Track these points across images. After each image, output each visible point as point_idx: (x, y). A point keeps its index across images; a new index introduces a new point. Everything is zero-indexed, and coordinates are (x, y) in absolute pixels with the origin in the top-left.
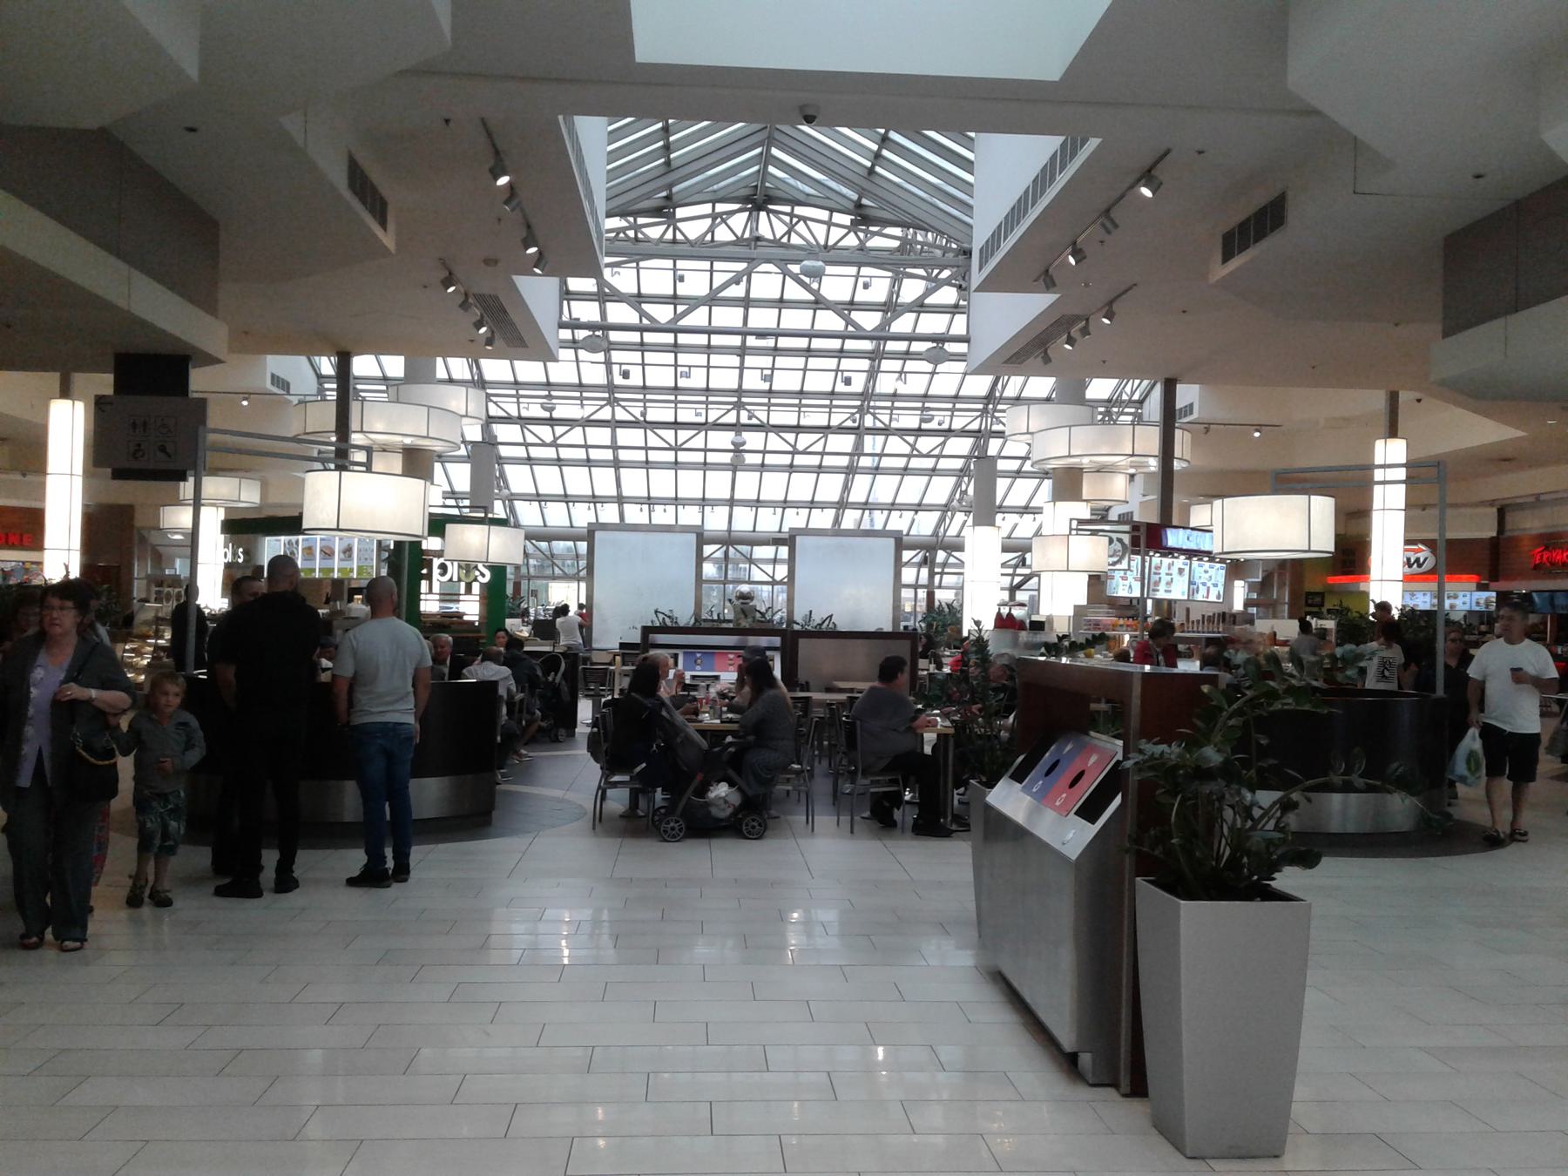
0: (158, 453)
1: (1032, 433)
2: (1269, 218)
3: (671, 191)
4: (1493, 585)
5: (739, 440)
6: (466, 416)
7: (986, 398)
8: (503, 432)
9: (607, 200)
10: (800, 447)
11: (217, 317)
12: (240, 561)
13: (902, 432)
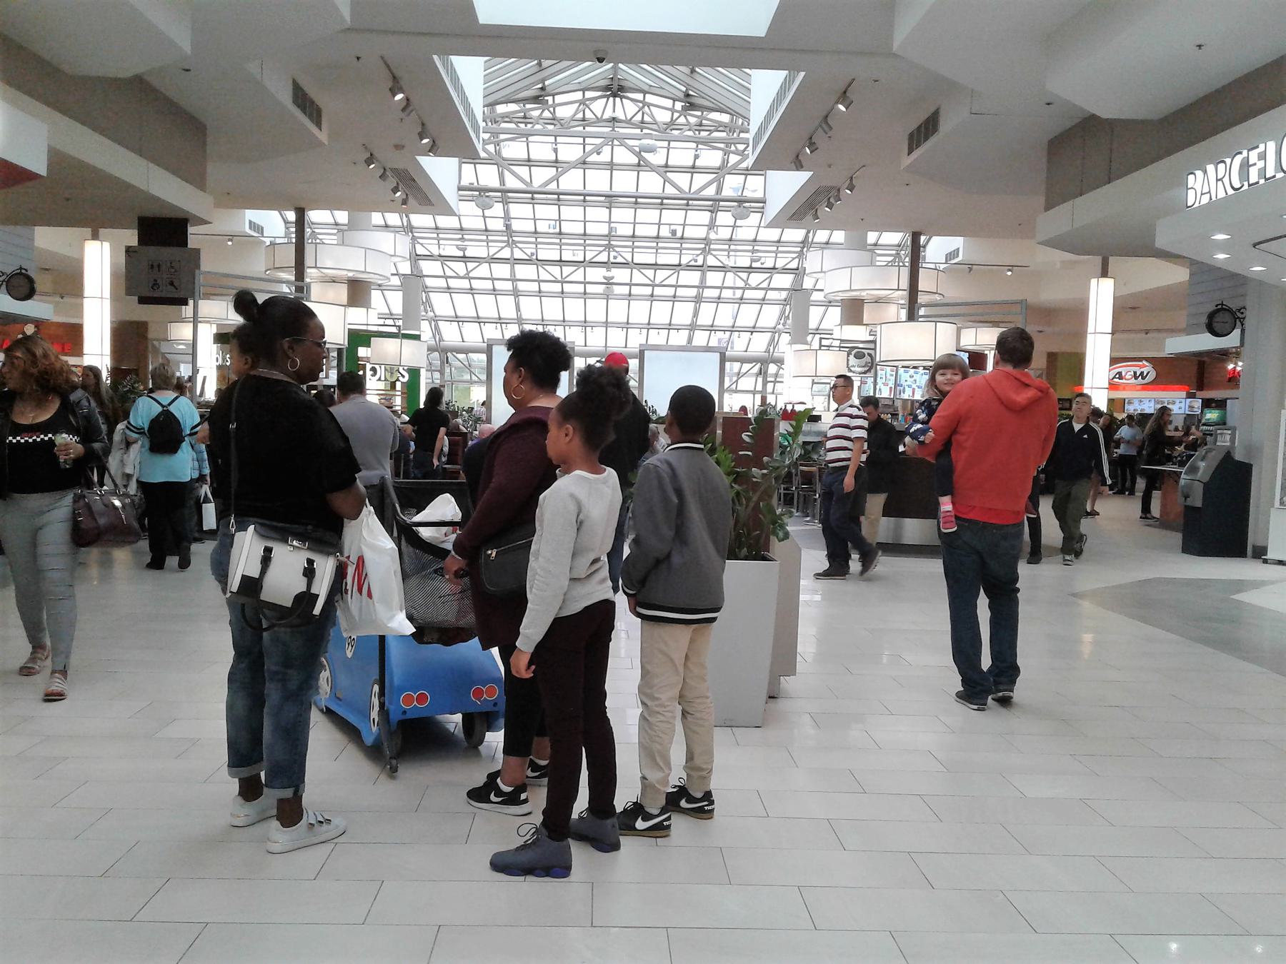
0: (169, 287)
1: (825, 272)
2: (929, 127)
3: (544, 84)
4: (1199, 394)
5: (609, 274)
6: (395, 256)
7: (802, 242)
8: (428, 267)
9: (484, 97)
10: (657, 282)
12: (228, 364)
13: (737, 269)
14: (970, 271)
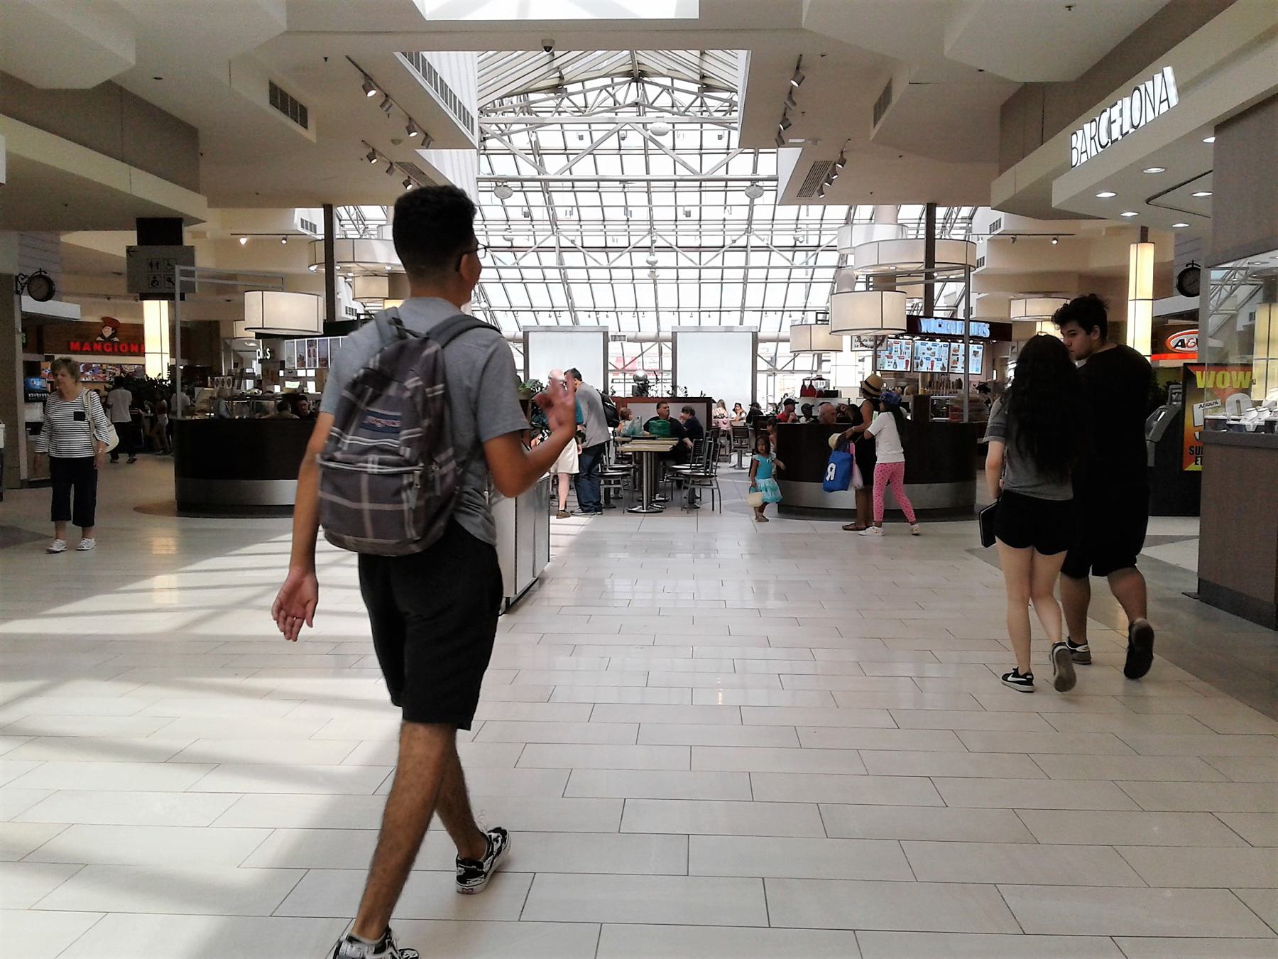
5: (652, 259)
11: (199, 193)
13: (782, 248)
14: (1014, 242)
